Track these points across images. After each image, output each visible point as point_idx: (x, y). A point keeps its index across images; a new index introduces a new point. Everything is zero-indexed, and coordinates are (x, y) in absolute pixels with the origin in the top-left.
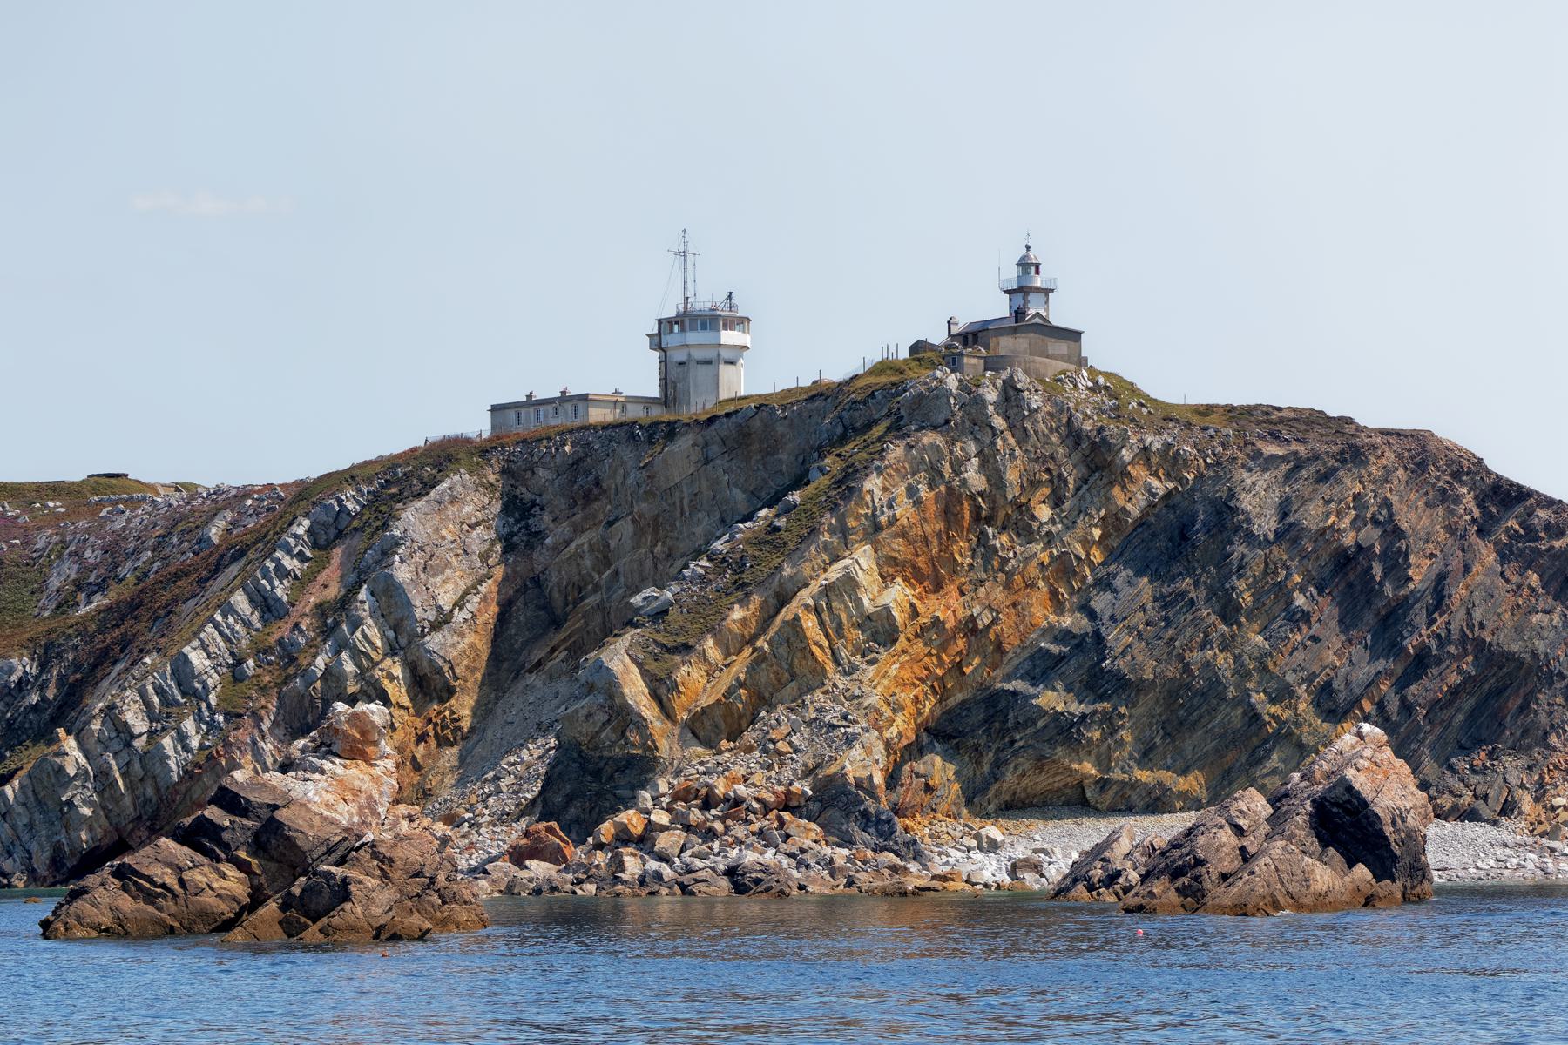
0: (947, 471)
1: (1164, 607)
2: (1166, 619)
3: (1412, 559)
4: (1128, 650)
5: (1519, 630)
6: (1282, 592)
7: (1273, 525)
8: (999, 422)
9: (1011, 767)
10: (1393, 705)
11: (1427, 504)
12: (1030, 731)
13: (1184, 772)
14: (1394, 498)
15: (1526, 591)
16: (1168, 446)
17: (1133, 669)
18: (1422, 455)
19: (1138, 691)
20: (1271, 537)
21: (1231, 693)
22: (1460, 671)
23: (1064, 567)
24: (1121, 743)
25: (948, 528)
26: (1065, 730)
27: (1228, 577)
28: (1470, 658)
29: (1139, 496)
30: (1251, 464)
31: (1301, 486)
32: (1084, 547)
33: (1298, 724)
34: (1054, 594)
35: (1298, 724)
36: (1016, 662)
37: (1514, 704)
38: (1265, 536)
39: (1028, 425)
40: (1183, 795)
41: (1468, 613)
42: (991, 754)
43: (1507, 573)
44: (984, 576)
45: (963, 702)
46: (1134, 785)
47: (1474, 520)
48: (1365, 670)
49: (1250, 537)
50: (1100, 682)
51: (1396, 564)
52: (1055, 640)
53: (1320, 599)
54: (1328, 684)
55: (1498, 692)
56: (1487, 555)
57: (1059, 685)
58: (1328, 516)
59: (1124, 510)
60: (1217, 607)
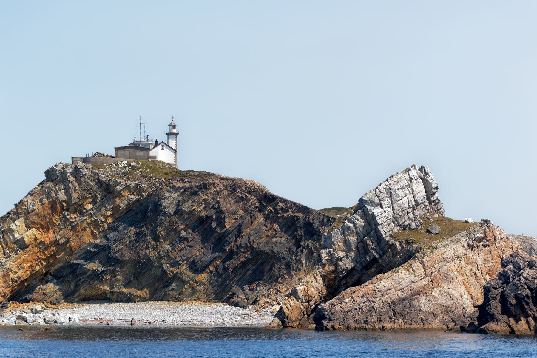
0: (53, 194)
1: (136, 237)
2: (136, 240)
3: (227, 220)
4: (122, 250)
5: (268, 243)
6: (177, 232)
7: (174, 209)
8: (71, 179)
9: (82, 287)
10: (220, 269)
11: (235, 202)
12: (85, 276)
13: (141, 289)
14: (221, 201)
15: (272, 230)
16: (137, 185)
17: (121, 256)
18: (234, 187)
19: (124, 263)
20: (172, 213)
21: (156, 264)
22: (245, 257)
23: (96, 224)
24: (118, 280)
26: (97, 276)
27: (156, 227)
28: (249, 253)
29: (125, 201)
30: (171, 190)
31: (185, 197)
32: (104, 218)
33: (181, 274)
34: (92, 232)
36: (79, 254)
37: (267, 268)
38: (170, 213)
39: (82, 180)
40: (139, 297)
41: (249, 238)
42: (73, 283)
43: (267, 225)
44: (63, 227)
45: (62, 267)
46: (122, 293)
47: (256, 207)
48: (210, 256)
49: (165, 214)
50: (111, 261)
51: (221, 222)
52: (94, 247)
53: (193, 233)
54: (194, 261)
55: (262, 264)
56: (260, 218)
57: (97, 261)
58: (193, 206)
59: (119, 205)
60: (153, 236)
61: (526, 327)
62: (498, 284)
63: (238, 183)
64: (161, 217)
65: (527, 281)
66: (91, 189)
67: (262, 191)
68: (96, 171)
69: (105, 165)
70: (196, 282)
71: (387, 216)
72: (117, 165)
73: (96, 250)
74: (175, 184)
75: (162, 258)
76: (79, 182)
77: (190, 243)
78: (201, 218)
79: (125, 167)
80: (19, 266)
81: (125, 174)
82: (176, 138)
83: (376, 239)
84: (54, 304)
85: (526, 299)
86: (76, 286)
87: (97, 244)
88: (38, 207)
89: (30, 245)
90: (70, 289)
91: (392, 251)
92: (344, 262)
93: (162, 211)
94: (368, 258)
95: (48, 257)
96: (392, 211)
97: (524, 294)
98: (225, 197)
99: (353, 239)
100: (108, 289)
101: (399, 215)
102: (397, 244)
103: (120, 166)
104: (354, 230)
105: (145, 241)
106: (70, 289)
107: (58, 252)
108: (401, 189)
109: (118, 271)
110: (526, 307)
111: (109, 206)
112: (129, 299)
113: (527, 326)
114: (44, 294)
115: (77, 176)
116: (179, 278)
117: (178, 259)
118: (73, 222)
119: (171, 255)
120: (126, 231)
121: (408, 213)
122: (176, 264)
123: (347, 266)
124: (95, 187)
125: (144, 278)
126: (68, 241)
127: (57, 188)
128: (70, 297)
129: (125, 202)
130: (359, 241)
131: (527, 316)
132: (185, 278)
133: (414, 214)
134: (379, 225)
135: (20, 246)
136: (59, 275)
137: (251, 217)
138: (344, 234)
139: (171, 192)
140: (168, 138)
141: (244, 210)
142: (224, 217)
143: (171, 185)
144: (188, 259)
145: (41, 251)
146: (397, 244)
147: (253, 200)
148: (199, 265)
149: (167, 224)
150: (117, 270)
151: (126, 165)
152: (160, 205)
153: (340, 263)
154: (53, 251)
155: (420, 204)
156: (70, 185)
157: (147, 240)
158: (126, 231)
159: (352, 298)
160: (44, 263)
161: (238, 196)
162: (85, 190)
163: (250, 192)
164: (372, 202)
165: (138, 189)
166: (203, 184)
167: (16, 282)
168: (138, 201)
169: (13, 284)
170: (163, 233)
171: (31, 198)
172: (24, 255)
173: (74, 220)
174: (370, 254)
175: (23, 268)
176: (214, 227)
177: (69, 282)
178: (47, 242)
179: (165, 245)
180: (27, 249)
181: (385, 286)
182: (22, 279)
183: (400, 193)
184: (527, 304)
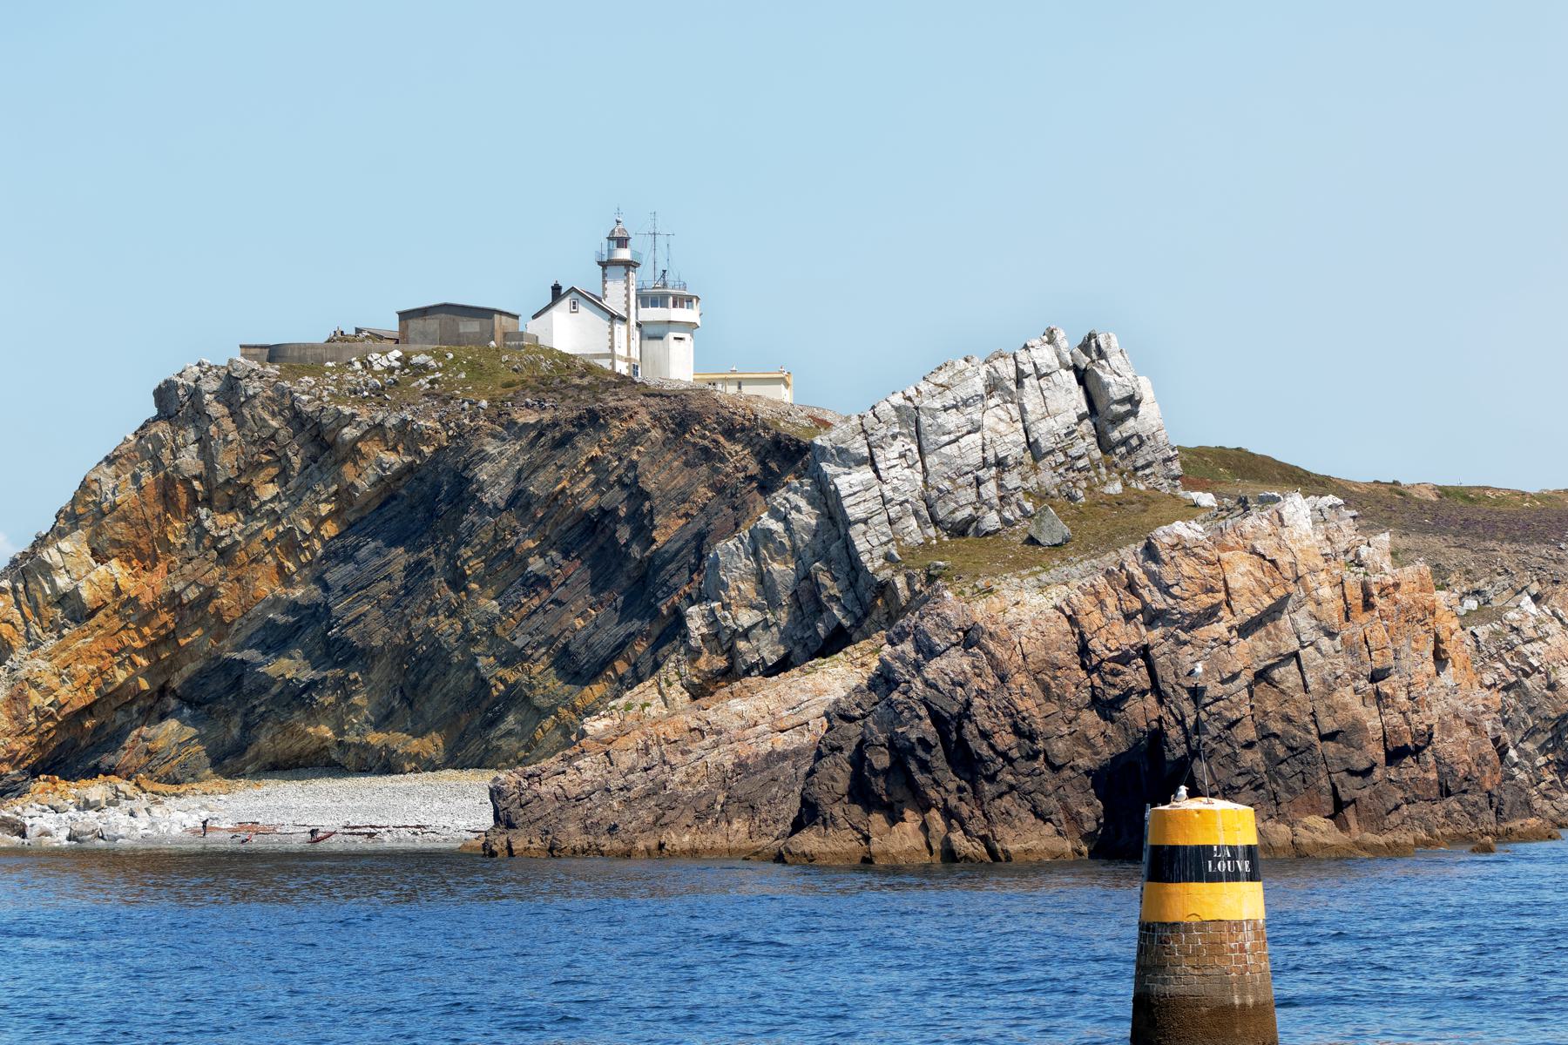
0: (166, 454)
3: (658, 520)
7: (507, 492)
8: (216, 409)
11: (686, 464)
12: (264, 697)
13: (419, 734)
16: (404, 422)
20: (502, 504)
21: (457, 657)
23: (291, 543)
24: (355, 709)
25: (167, 510)
26: (298, 697)
29: (370, 471)
32: (311, 523)
33: (531, 687)
35: (531, 687)
39: (246, 411)
44: (195, 553)
45: (201, 671)
46: (367, 747)
47: (750, 478)
51: (642, 528)
52: (286, 613)
53: (565, 563)
54: (566, 646)
57: (297, 653)
59: (352, 484)
60: (449, 575)
61: (918, 841)
62: (859, 705)
63: (694, 405)
64: (471, 518)
65: (930, 693)
66: (272, 437)
67: (766, 428)
68: (287, 384)
69: (330, 364)
70: (574, 710)
71: (889, 494)
72: (367, 365)
73: (291, 619)
74: (515, 416)
75: (473, 641)
76: (238, 419)
77: (559, 593)
78: (586, 515)
79: (391, 370)
80: (57, 673)
81: (378, 391)
82: (627, 274)
83: (847, 569)
84: (177, 782)
85: (920, 752)
86: (246, 727)
87: (295, 603)
88: (127, 496)
89: (99, 609)
90: (228, 738)
91: (887, 604)
92: (755, 643)
93: (474, 497)
94: (821, 629)
95: (153, 645)
96: (919, 478)
97: (913, 736)
98: (657, 449)
99: (781, 570)
100: (330, 734)
101: (940, 490)
102: (900, 581)
103: (377, 367)
104: (786, 541)
105: (429, 591)
106: (228, 738)
107: (181, 628)
108: (955, 406)
109: (356, 681)
110: (920, 778)
111: (326, 487)
112: (387, 765)
113: (923, 839)
114: (149, 752)
115: (233, 400)
116: (527, 698)
117: (519, 643)
118: (222, 538)
119: (498, 630)
120: (378, 562)
121: (979, 482)
122: (514, 657)
123: (765, 654)
124: (282, 432)
125: (428, 700)
126: (210, 594)
127: (180, 440)
128: (231, 761)
129: (371, 474)
130: (802, 575)
131: (924, 806)
132: (539, 700)
133: (1000, 486)
134: (850, 524)
135: (73, 612)
136: (196, 696)
137: (735, 508)
138: (756, 553)
139: (504, 439)
140: (604, 275)
141: (712, 487)
142: (651, 511)
143: (504, 419)
144: (551, 641)
145: (131, 625)
146: (900, 581)
147: (738, 456)
148: (583, 658)
149: (486, 537)
150: (352, 677)
151: (397, 364)
152: (470, 481)
153: (742, 645)
154: (165, 625)
155: (1051, 452)
156: (213, 428)
157: (432, 586)
158: (378, 562)
159: (607, 754)
160: (142, 661)
161: (695, 445)
162: (254, 443)
163: (730, 433)
164: (841, 451)
165: (406, 435)
166: (589, 411)
167: (51, 717)
168: (409, 469)
169: (39, 724)
170: (475, 566)
171: (110, 471)
172: (81, 640)
173: (222, 533)
174: (825, 615)
175: (72, 677)
176: (622, 542)
177: (228, 715)
178: (147, 598)
179: (483, 601)
180: (92, 622)
181: (742, 717)
182: (68, 710)
183: (952, 420)
184: (925, 767)
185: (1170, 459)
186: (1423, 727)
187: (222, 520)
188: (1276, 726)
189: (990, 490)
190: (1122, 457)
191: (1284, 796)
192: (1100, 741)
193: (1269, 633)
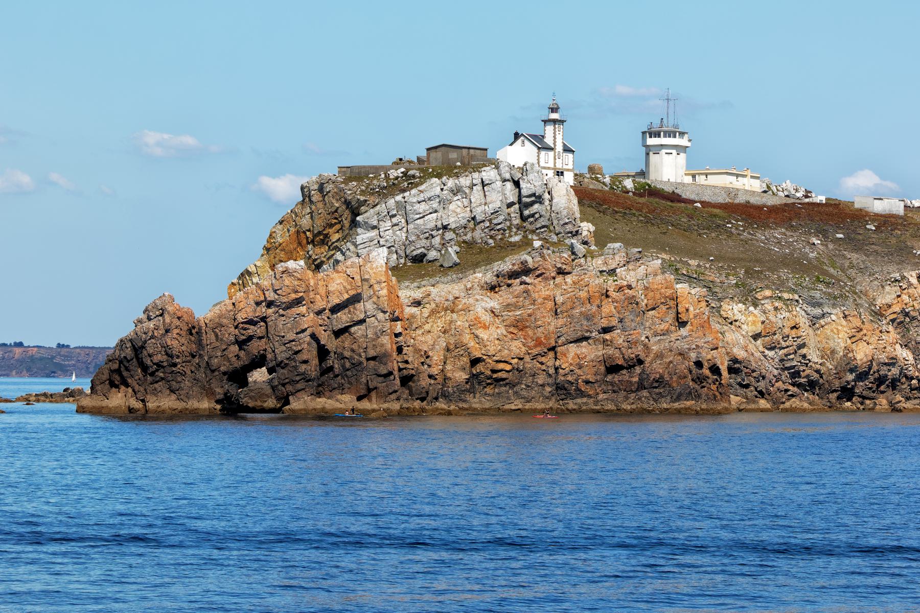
66: (336, 211)
96: (404, 235)
131: (127, 385)
164: (366, 223)
171: (280, 227)
183: (423, 207)
185: (566, 224)
186: (633, 356)
187: (318, 250)
188: (347, 354)
189: (437, 241)
190: (531, 223)
191: (347, 385)
192: (234, 359)
193: (350, 311)
